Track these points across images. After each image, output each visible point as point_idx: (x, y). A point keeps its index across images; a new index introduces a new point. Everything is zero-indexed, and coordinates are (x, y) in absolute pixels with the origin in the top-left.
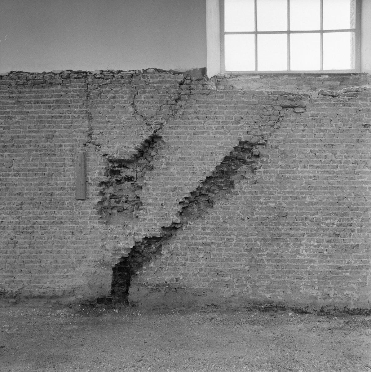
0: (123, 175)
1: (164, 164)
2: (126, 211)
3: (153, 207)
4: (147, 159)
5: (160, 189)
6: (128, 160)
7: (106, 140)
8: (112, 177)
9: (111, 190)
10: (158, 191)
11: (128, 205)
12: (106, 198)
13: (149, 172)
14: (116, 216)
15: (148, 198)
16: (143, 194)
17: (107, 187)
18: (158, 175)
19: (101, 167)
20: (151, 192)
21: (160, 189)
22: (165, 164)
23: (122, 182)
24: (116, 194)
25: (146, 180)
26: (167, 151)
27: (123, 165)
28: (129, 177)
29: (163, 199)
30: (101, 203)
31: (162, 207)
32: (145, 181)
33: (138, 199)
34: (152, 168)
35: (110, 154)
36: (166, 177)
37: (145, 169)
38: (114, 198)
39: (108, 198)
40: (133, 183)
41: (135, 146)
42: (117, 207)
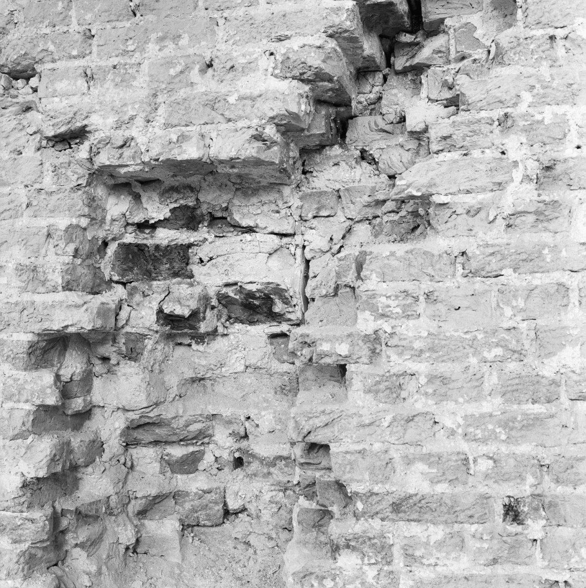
0: (210, 279)
1: (517, 175)
2: (238, 527)
3: (437, 533)
4: (373, 162)
5: (492, 380)
6: (232, 162)
7: (74, 27)
8: (131, 294)
9: (122, 391)
10: (478, 399)
11: (257, 485)
12: (97, 447)
13: (401, 249)
14: (175, 557)
15: (396, 455)
16: (354, 419)
17: (99, 368)
18: (474, 273)
19: (43, 223)
20: (419, 407)
21: (492, 380)
22: (527, 178)
23: (203, 328)
24: (167, 412)
25: (373, 309)
26: (544, 69)
27: (204, 209)
28: (251, 295)
29: (522, 463)
30: (62, 477)
31: (514, 528)
32: (366, 323)
33: (314, 458)
34: (417, 216)
35: (101, 124)
36: (538, 280)
37: (362, 231)
38: (156, 443)
39: (113, 445)
40: (283, 335)
41: (281, 49)
42: (177, 496)
